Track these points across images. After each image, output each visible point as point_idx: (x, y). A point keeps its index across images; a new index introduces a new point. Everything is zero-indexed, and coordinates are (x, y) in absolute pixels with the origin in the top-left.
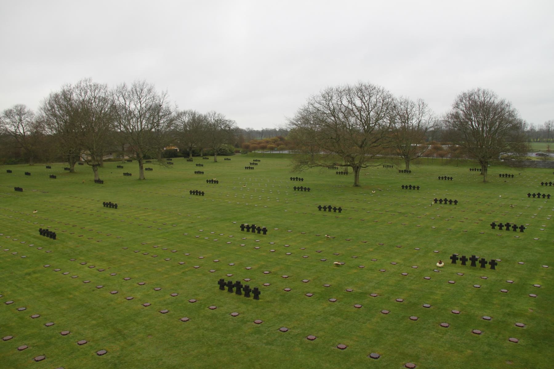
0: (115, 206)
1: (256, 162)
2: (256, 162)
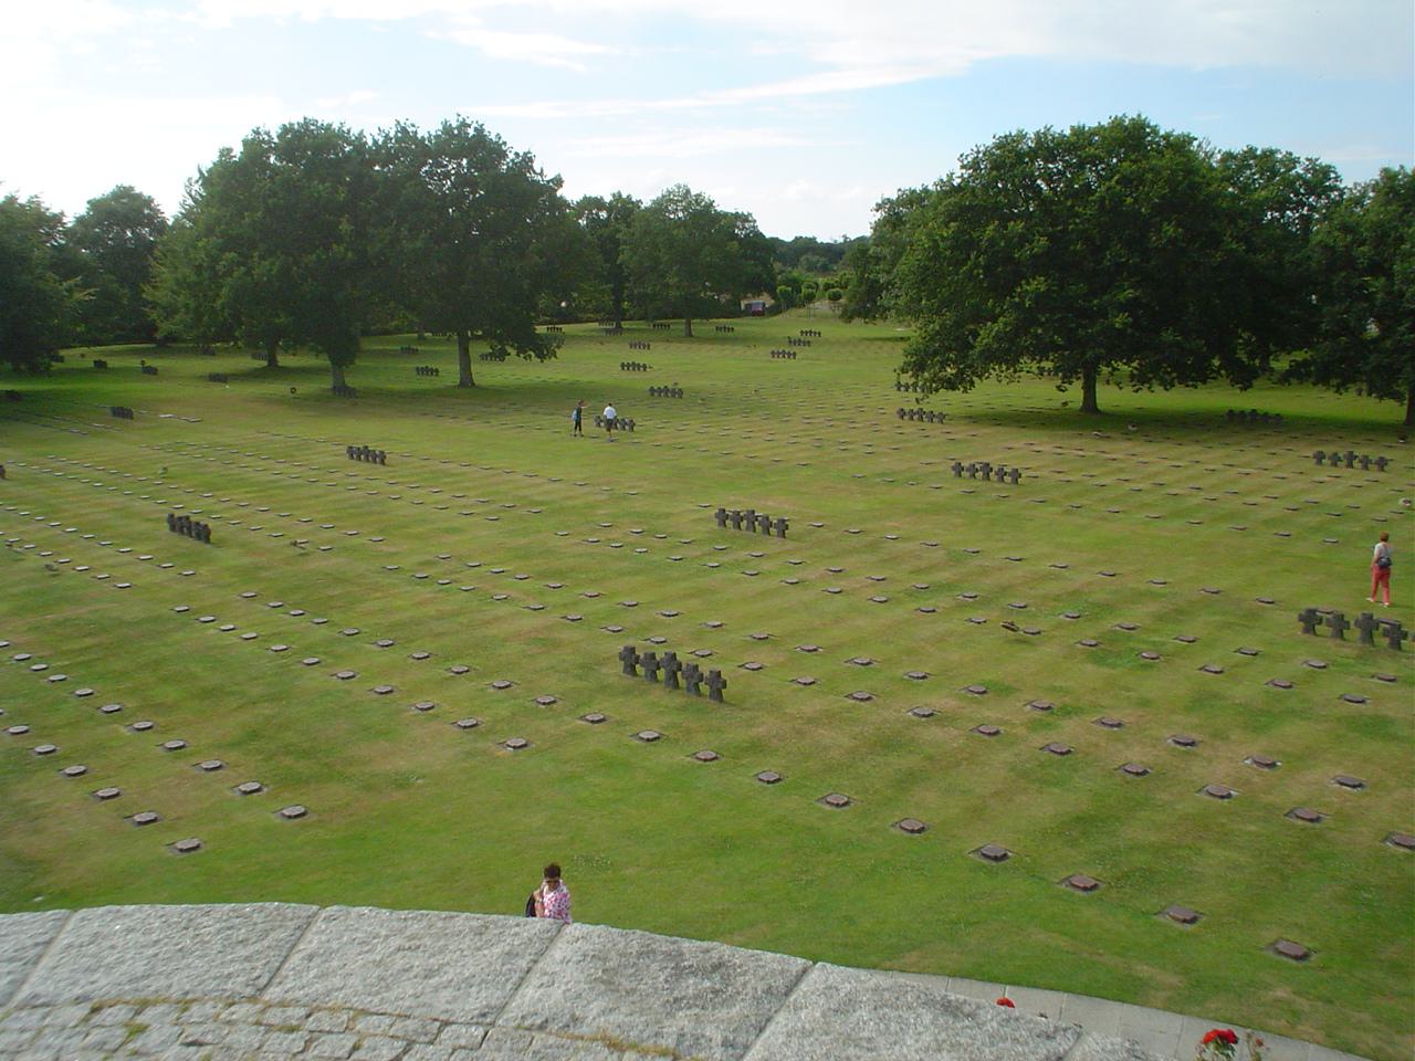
0: (380, 458)
1: (808, 338)
2: (808, 338)
